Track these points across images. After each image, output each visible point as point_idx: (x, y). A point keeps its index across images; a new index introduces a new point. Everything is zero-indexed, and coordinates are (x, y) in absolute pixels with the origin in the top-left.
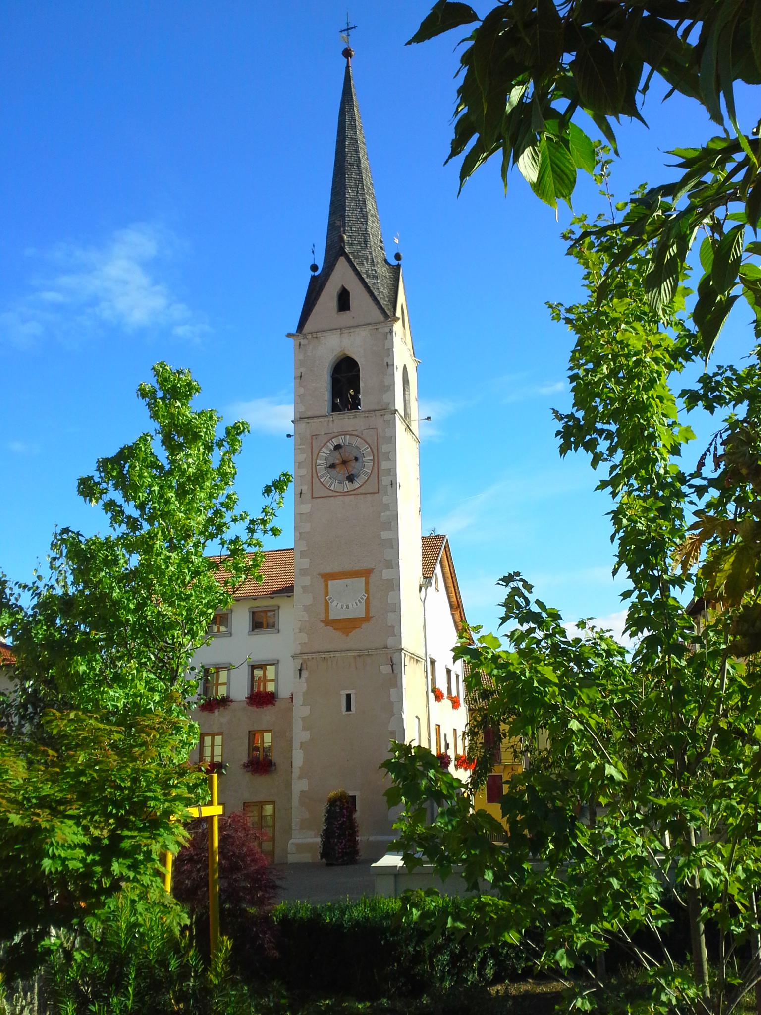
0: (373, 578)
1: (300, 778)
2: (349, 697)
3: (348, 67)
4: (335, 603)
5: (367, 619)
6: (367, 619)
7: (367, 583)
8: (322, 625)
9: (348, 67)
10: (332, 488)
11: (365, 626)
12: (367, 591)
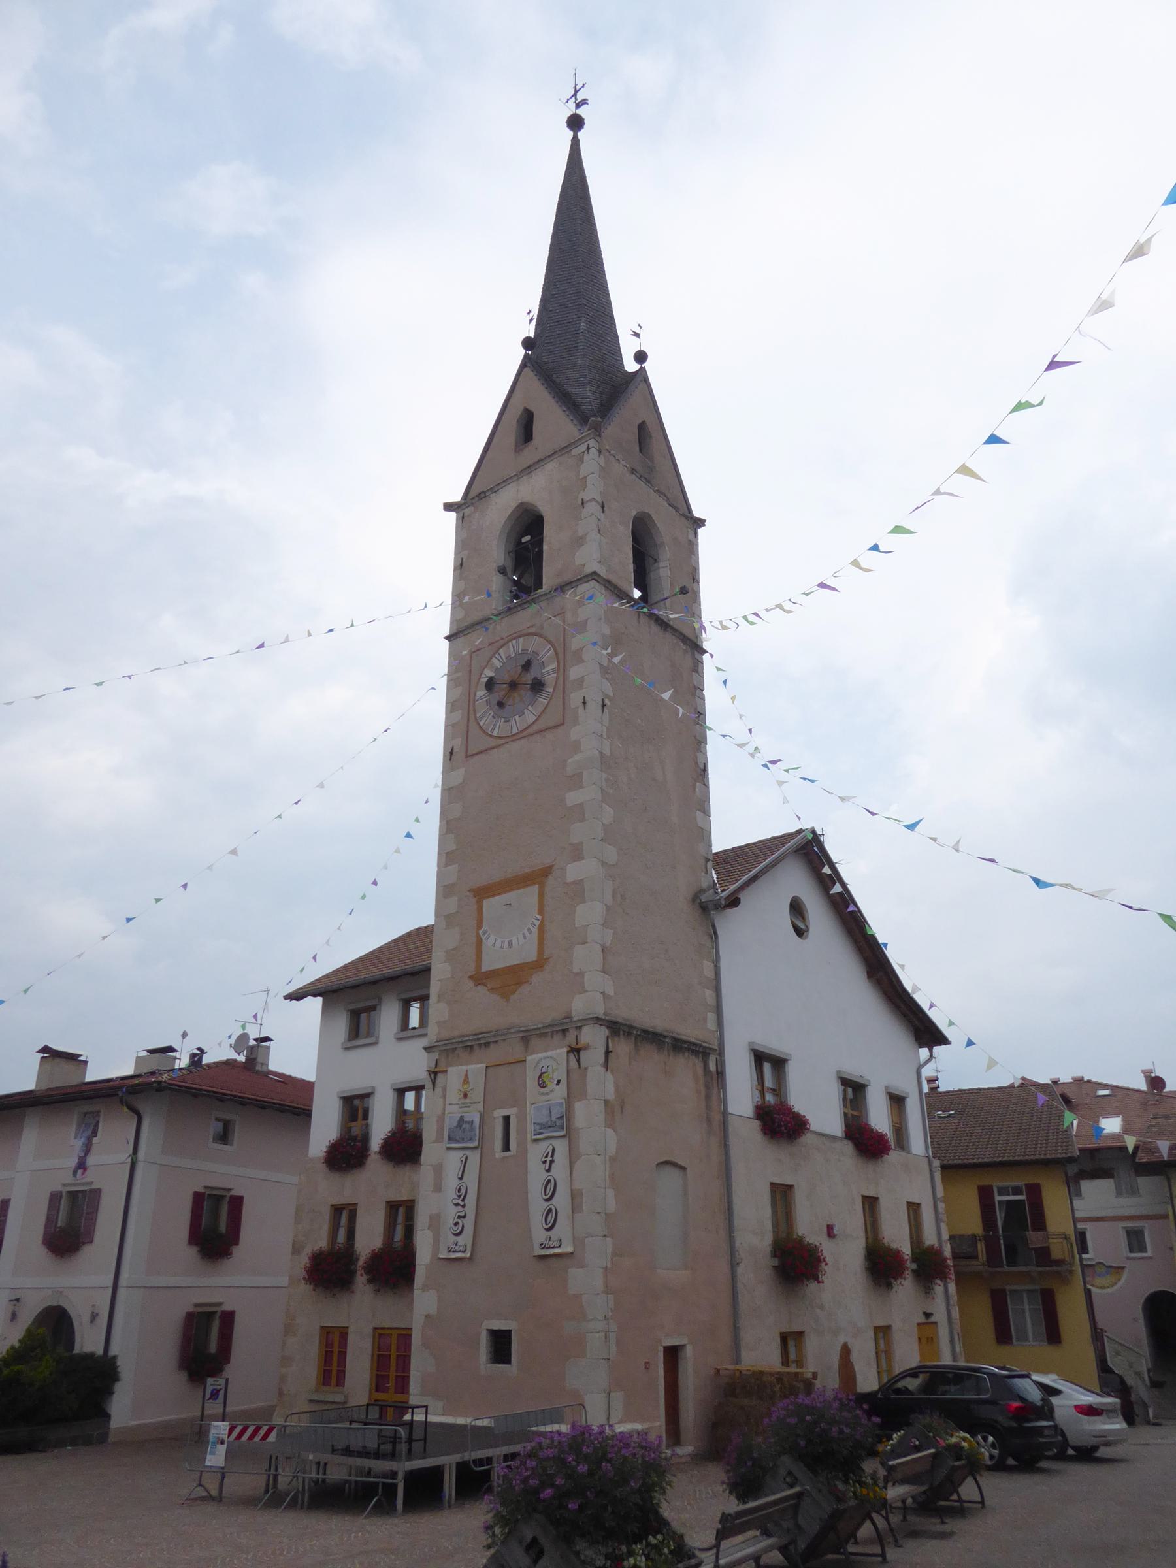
0: (550, 882)
1: (425, 1288)
2: (507, 1119)
3: (575, 143)
5: (539, 964)
6: (539, 964)
7: (541, 894)
8: (471, 984)
9: (575, 143)
10: (495, 733)
11: (536, 979)
12: (541, 911)
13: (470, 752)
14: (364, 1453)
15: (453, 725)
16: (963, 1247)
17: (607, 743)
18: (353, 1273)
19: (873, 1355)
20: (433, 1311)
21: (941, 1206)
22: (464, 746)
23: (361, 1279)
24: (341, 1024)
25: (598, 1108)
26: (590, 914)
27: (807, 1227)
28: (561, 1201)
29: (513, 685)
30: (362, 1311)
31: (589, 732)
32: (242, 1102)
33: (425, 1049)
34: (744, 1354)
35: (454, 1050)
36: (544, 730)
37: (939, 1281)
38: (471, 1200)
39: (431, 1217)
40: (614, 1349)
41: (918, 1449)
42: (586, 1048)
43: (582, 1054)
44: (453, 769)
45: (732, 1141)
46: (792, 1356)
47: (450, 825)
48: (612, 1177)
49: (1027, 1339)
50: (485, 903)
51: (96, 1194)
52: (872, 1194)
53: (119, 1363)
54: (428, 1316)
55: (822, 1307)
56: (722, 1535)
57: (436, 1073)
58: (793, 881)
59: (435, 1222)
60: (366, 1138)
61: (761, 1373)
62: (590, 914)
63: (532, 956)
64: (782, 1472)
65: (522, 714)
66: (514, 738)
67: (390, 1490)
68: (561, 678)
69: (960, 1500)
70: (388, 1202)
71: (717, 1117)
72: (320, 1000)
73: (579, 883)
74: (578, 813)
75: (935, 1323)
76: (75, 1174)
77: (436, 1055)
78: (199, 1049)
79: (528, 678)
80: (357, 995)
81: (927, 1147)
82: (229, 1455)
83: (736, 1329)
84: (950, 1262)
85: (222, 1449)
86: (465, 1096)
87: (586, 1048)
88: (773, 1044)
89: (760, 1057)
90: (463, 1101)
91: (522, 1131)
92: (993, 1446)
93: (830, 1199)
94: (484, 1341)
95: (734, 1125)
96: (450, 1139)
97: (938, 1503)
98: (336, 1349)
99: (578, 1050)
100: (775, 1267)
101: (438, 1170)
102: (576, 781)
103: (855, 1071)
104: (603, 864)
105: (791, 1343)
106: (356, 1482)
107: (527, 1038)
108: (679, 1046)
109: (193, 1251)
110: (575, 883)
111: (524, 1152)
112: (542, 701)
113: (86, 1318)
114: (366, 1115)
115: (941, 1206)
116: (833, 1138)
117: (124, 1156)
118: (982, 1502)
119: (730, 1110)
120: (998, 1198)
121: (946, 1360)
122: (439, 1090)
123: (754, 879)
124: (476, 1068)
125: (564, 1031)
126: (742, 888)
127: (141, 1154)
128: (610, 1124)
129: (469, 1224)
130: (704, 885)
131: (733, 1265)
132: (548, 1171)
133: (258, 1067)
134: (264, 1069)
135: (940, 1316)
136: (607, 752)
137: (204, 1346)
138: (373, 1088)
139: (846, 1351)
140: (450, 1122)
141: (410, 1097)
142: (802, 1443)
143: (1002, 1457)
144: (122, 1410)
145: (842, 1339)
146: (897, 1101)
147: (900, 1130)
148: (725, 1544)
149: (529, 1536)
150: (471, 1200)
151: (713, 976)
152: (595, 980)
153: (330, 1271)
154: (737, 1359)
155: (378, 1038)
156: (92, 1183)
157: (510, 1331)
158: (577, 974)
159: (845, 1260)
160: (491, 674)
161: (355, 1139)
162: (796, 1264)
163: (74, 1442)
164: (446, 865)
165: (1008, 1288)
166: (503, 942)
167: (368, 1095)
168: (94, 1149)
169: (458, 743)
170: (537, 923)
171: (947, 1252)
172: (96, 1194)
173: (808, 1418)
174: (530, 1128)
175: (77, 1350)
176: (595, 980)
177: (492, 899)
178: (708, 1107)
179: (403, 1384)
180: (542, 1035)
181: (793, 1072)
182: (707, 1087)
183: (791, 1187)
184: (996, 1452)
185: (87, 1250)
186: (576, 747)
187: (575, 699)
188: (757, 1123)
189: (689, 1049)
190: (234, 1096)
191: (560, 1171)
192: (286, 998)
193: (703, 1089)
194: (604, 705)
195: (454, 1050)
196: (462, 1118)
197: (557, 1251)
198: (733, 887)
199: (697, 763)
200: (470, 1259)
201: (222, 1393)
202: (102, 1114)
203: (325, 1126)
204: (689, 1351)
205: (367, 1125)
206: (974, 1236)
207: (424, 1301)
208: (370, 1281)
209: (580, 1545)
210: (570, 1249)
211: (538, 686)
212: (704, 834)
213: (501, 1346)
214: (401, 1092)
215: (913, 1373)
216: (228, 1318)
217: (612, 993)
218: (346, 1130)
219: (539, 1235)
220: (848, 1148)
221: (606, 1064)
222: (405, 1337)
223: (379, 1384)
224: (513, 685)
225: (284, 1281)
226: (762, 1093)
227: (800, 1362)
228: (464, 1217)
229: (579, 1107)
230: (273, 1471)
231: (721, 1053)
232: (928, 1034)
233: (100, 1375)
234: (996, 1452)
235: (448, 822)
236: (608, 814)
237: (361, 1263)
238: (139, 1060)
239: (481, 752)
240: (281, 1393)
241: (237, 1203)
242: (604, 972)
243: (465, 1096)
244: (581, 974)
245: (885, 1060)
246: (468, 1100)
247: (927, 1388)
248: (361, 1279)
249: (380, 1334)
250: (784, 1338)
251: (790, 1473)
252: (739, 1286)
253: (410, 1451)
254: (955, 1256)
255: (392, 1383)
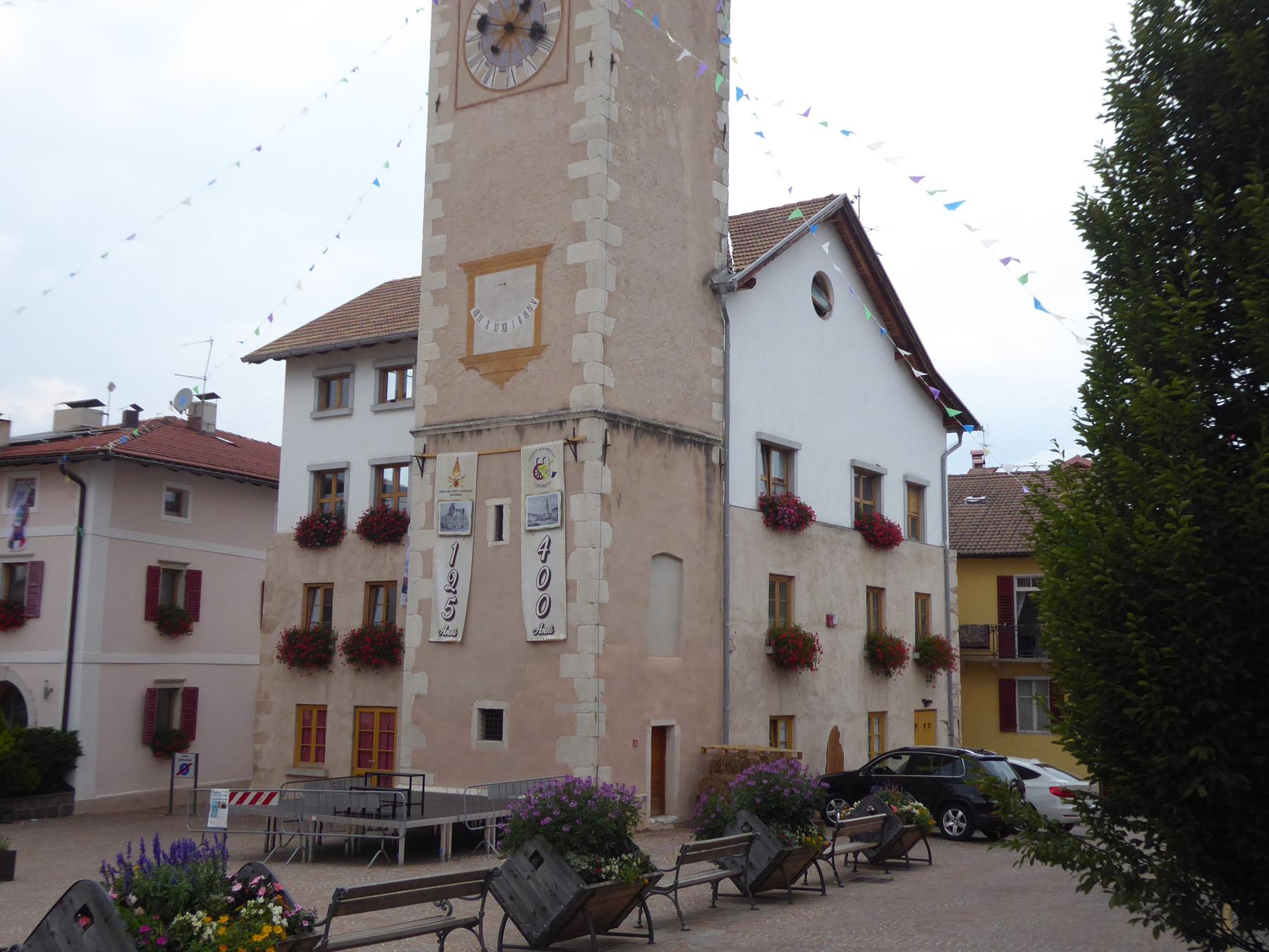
0: (550, 262)
1: (415, 669)
2: (500, 509)
4: (484, 322)
5: (536, 351)
6: (536, 351)
7: (539, 276)
8: (462, 367)
10: (489, 85)
11: (532, 367)
12: (539, 293)
13: (460, 104)
14: (364, 814)
15: (440, 69)
16: (973, 638)
17: (615, 107)
18: (330, 653)
19: (866, 739)
20: (424, 691)
21: (953, 597)
22: (452, 99)
23: (339, 659)
24: (309, 393)
25: (595, 502)
26: (591, 300)
27: (805, 617)
28: (556, 590)
29: (510, 28)
30: (343, 691)
31: (595, 92)
32: (197, 472)
33: (412, 433)
34: (731, 735)
35: (444, 435)
36: (545, 87)
37: (941, 670)
38: (463, 588)
39: (420, 602)
40: (603, 728)
41: (872, 813)
42: (583, 441)
43: (579, 446)
44: (440, 123)
45: (732, 534)
46: (781, 736)
47: (437, 189)
48: (607, 569)
49: (1032, 728)
50: (478, 280)
51: (37, 568)
52: (878, 584)
53: (79, 739)
54: (418, 696)
55: (815, 694)
56: (682, 860)
57: (424, 459)
58: (824, 254)
59: (425, 607)
60: (341, 516)
61: (746, 751)
62: (591, 300)
63: (529, 342)
64: (740, 823)
65: (519, 64)
66: (510, 92)
67: (392, 848)
68: (566, 26)
69: (907, 859)
70: (367, 583)
71: (717, 509)
72: (284, 362)
73: (580, 267)
74: (581, 187)
75: (935, 710)
76: (11, 545)
77: (423, 441)
78: (134, 406)
79: (527, 21)
80: (328, 359)
81: (944, 537)
82: (231, 818)
83: (725, 712)
84: (956, 652)
85: (224, 813)
86: (456, 484)
87: (583, 441)
88: (782, 433)
89: (767, 448)
90: (453, 488)
91: (515, 521)
92: (962, 819)
93: (831, 589)
94: (475, 719)
95: (736, 519)
96: (443, 527)
97: (887, 855)
98: (314, 727)
99: (575, 443)
100: (768, 655)
101: (428, 556)
102: (579, 151)
103: (869, 459)
104: (607, 246)
105: (781, 725)
106: (356, 839)
107: (521, 428)
108: (681, 437)
109: (151, 627)
110: (577, 266)
111: (515, 535)
112: (543, 51)
113: (39, 693)
114: (341, 487)
115: (953, 597)
116: (842, 529)
117: (72, 528)
118: (930, 861)
119: (732, 502)
120: (1017, 589)
121: (943, 743)
122: (427, 476)
123: (774, 256)
124: (467, 457)
125: (561, 423)
126: (758, 268)
127: (89, 527)
128: (606, 514)
129: (461, 610)
130: (717, 264)
131: (726, 652)
132: (544, 561)
133: (204, 428)
134: (211, 430)
135: (940, 703)
136: (615, 118)
137: (168, 723)
138: (348, 463)
139: (835, 734)
140: (439, 510)
141: (388, 474)
142: (758, 801)
143: (970, 829)
144: (86, 783)
145: (833, 724)
146: (916, 490)
147: (916, 523)
148: (683, 867)
149: (532, 851)
150: (463, 588)
151: (721, 364)
152: (596, 373)
153: (306, 650)
154: (725, 739)
155: (352, 409)
156: (31, 555)
157: (501, 711)
158: (576, 364)
159: (842, 652)
160: (485, 11)
161: (329, 516)
162: (790, 652)
163: (40, 815)
164: (433, 234)
165: (1017, 678)
166: (496, 325)
167: (342, 470)
168: (31, 519)
169: (445, 92)
170: (534, 307)
171: (955, 643)
172: (37, 568)
173: (765, 781)
174: (524, 520)
175: (31, 724)
176: (596, 373)
177: (484, 277)
178: (708, 500)
179: (388, 758)
180: (537, 426)
181: (802, 463)
182: (708, 479)
183: (791, 578)
184: (964, 825)
185: (33, 626)
186: (580, 111)
187: (580, 54)
188: (760, 515)
189: (690, 441)
190: (179, 461)
191: (556, 562)
192: (244, 360)
193: (704, 481)
194: (612, 62)
195: (444, 435)
196: (453, 507)
197: (550, 637)
198: (748, 268)
199: (716, 125)
200: (462, 643)
201: (192, 768)
202: (38, 482)
203: (295, 502)
204: (677, 732)
205: (342, 502)
206: (987, 627)
207: (413, 683)
208: (349, 661)
209: (570, 855)
210: (562, 636)
211: (538, 32)
212: (720, 205)
213: (492, 724)
214: (379, 469)
215: (896, 755)
216: (191, 696)
217: (612, 385)
218: (318, 506)
219: (532, 622)
220: (857, 538)
221: (604, 458)
222: (389, 717)
223: (362, 758)
224: (510, 28)
225: (255, 659)
226: (768, 483)
227: (788, 744)
228: (456, 603)
229: (575, 500)
230: (272, 831)
231: (725, 444)
232: (955, 416)
233: (60, 751)
234: (964, 825)
235: (435, 185)
236: (615, 188)
237: (339, 642)
238: (58, 414)
239: (472, 106)
240: (256, 768)
241: (194, 579)
242: (604, 363)
243: (456, 484)
244: (580, 365)
245: (908, 449)
246: (459, 488)
247: (908, 768)
248: (339, 659)
249: (362, 714)
250: (774, 722)
251: (746, 823)
252: (731, 673)
253: (409, 814)
254: (963, 646)
255: (375, 760)
